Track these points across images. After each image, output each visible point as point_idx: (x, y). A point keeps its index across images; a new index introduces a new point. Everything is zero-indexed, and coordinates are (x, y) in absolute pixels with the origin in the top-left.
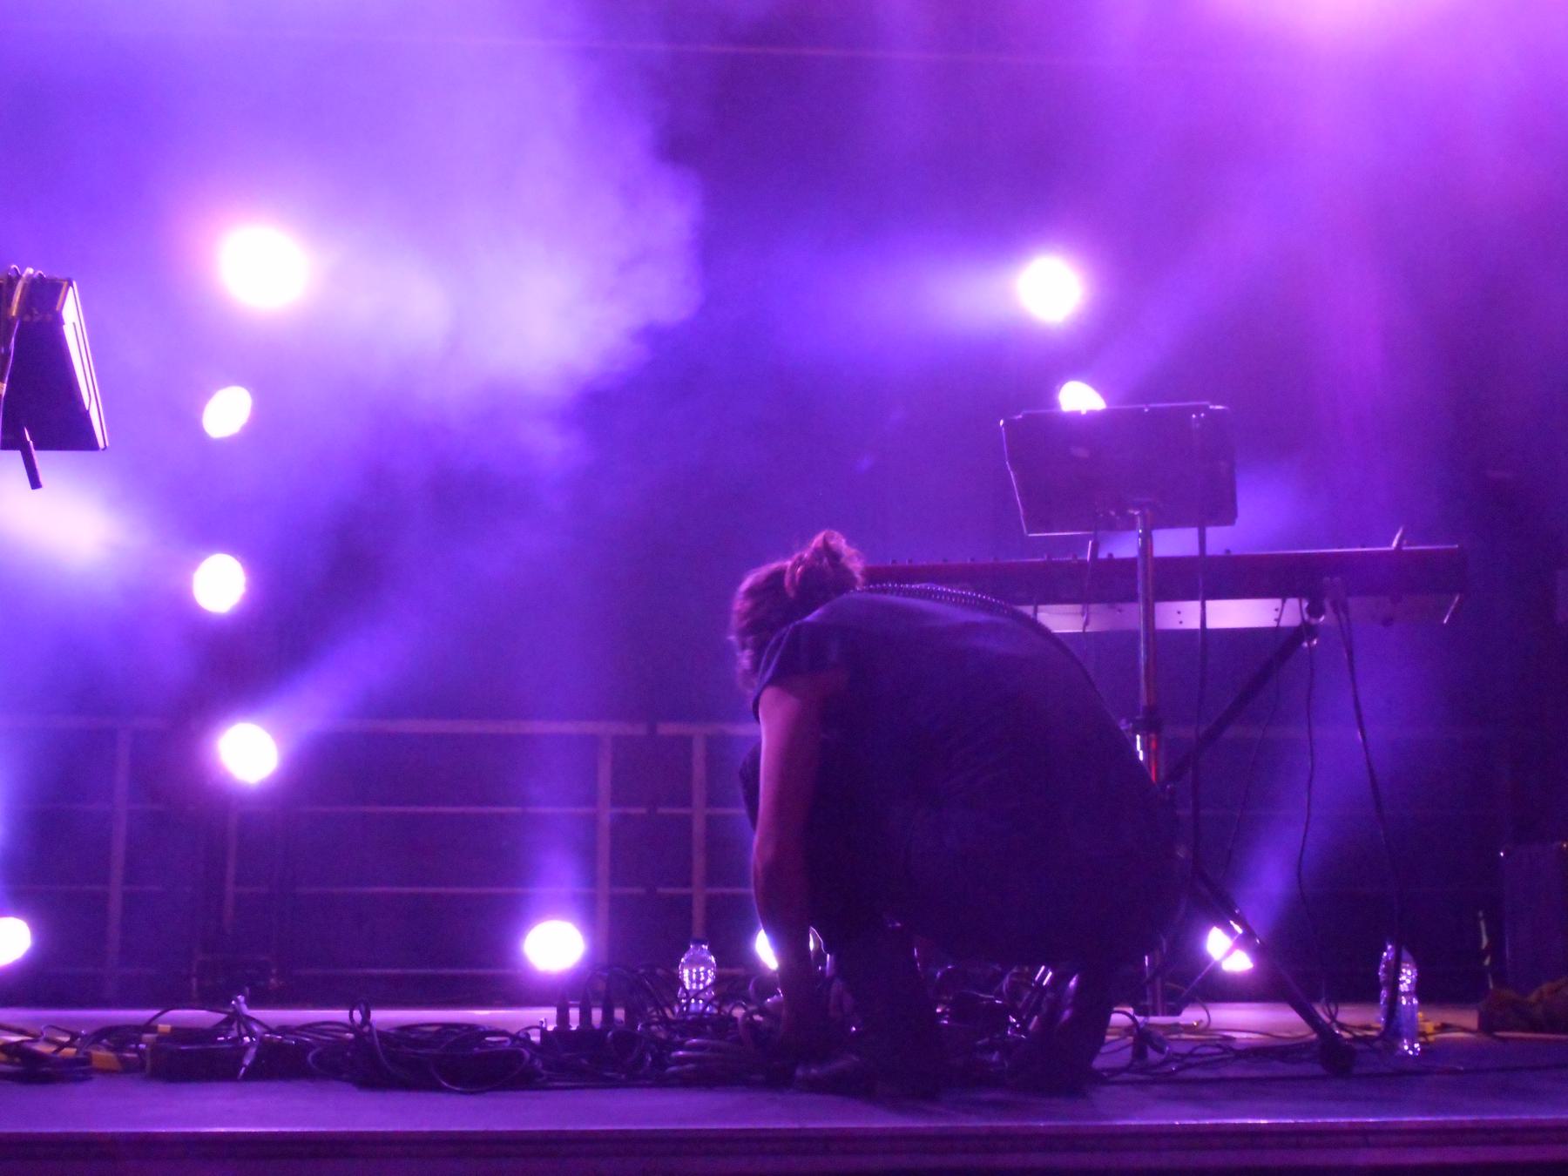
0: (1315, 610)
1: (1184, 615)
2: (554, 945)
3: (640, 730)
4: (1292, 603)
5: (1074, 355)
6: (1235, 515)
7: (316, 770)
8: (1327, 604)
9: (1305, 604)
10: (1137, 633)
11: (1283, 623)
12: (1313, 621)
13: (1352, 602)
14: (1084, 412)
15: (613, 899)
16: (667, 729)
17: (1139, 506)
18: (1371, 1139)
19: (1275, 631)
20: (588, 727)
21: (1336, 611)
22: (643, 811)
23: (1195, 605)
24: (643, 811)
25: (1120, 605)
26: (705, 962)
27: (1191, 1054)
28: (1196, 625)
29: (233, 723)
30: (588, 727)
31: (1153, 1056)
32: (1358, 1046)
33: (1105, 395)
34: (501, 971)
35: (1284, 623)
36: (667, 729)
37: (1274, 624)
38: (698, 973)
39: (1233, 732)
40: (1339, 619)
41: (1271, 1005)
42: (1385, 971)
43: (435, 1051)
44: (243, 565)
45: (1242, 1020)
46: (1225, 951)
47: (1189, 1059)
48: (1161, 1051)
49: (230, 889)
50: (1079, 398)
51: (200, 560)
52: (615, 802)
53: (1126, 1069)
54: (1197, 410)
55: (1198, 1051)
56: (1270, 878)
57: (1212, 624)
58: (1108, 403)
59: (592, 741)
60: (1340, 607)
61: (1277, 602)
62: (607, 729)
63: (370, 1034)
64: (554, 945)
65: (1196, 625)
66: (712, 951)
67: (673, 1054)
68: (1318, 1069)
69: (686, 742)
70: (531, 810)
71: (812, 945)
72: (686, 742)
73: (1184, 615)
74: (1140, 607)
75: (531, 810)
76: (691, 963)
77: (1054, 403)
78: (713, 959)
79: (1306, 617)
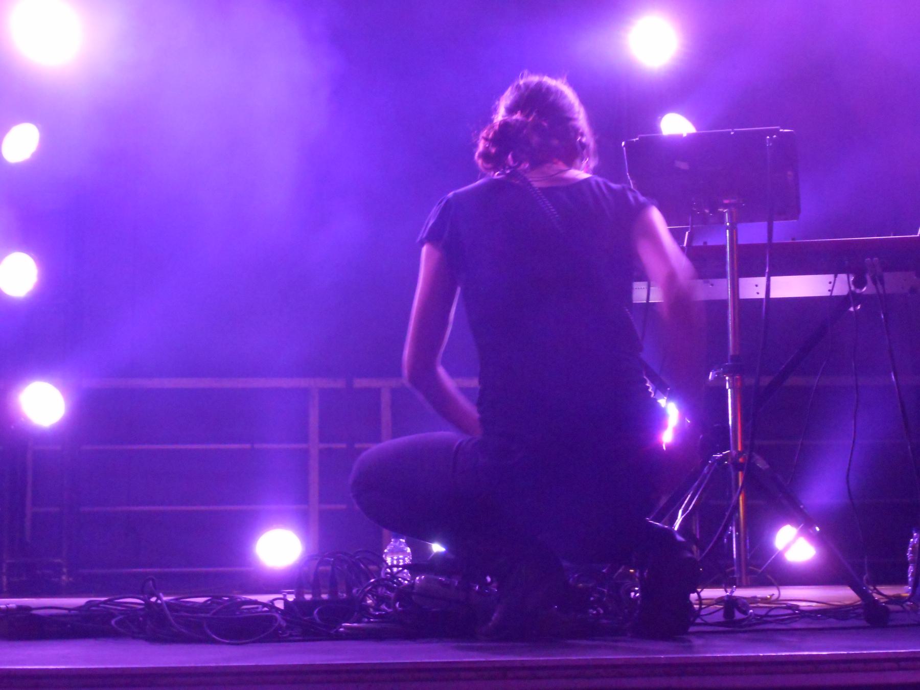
0: (859, 283)
1: (753, 288)
2: (279, 548)
3: (339, 384)
4: (843, 277)
5: (677, 91)
6: (799, 211)
7: (89, 412)
8: (868, 277)
9: (852, 278)
10: (724, 303)
11: (835, 293)
12: (858, 291)
13: (888, 277)
14: (685, 135)
15: (322, 513)
16: (360, 383)
17: (726, 206)
18: (903, 664)
19: (830, 298)
20: (303, 383)
21: (875, 283)
22: (344, 446)
23: (762, 281)
24: (344, 446)
25: (712, 281)
26: (403, 551)
27: (766, 615)
28: (762, 295)
29: (27, 384)
30: (303, 383)
31: (738, 616)
32: (892, 607)
33: (695, 124)
34: (237, 569)
35: (836, 293)
36: (360, 383)
37: (828, 294)
38: (398, 560)
39: (791, 381)
40: (877, 289)
41: (825, 587)
42: (912, 552)
43: (208, 615)
44: (35, 260)
45: (804, 596)
46: (794, 545)
47: (762, 619)
48: (745, 613)
49: (29, 510)
50: (675, 125)
51: (6, 254)
52: (322, 438)
53: (719, 624)
54: (771, 133)
55: (772, 613)
56: (825, 489)
57: (774, 294)
58: (697, 129)
59: (306, 391)
60: (878, 280)
61: (830, 277)
62: (315, 384)
63: (161, 604)
64: (279, 548)
65: (762, 295)
66: (408, 544)
67: (842, 285)
68: (863, 623)
69: (377, 392)
70: (257, 446)
71: (710, 377)
72: (377, 392)
73: (753, 288)
74: (728, 282)
75: (257, 446)
76: (392, 552)
77: (655, 129)
78: (409, 550)
79: (853, 288)
